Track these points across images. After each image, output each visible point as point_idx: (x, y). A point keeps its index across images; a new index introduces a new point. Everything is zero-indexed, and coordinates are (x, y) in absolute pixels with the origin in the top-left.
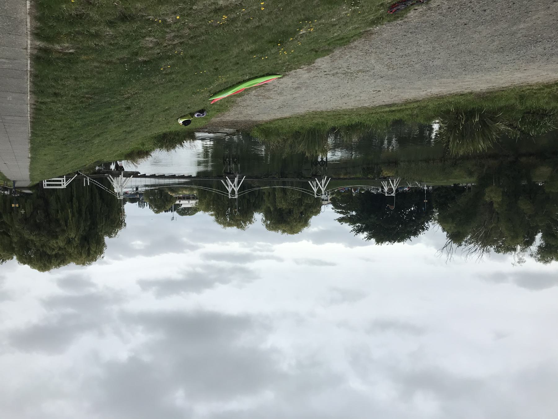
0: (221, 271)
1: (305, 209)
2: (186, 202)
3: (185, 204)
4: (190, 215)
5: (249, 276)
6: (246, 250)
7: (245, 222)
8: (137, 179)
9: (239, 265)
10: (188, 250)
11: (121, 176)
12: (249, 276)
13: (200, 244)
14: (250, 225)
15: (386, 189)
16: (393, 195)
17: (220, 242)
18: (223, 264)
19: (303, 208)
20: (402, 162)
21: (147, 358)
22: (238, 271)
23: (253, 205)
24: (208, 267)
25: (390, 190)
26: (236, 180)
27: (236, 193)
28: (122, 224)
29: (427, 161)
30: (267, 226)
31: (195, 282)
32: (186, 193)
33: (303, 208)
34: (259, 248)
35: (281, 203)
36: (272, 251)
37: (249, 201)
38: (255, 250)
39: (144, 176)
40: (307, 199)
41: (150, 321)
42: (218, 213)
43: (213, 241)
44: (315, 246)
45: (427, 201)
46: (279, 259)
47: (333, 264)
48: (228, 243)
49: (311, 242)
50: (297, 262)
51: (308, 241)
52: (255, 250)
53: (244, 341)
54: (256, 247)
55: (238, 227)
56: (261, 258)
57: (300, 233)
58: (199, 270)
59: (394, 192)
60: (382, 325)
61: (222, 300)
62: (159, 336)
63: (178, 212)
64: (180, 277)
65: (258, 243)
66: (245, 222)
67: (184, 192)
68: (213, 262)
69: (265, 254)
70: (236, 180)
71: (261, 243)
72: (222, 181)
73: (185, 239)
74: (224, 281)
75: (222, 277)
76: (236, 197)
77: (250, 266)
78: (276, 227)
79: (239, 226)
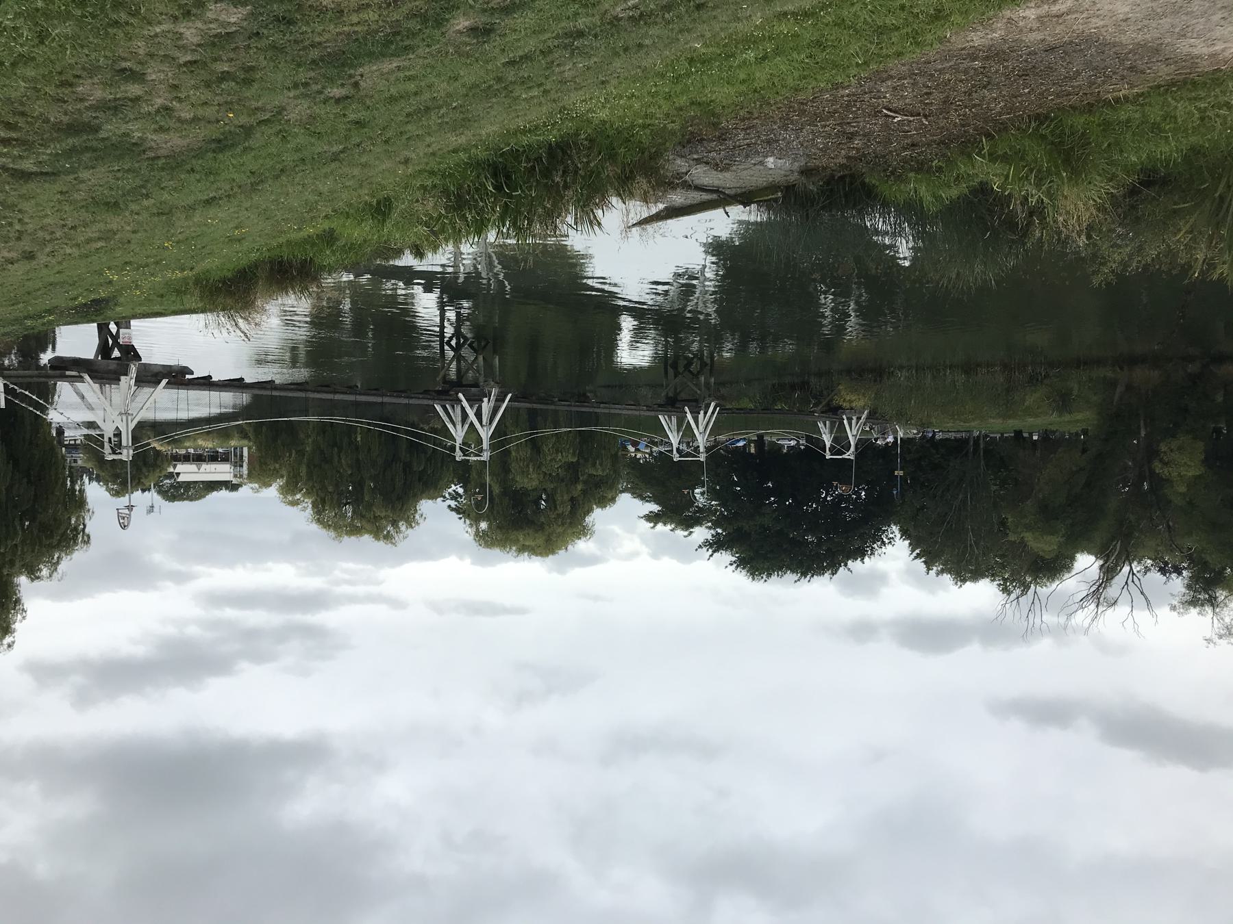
0: (251, 634)
1: (584, 492)
2: (191, 467)
3: (187, 472)
4: (191, 499)
5: (321, 643)
6: (314, 583)
7: (395, 524)
8: (183, 393)
9: (299, 618)
10: (169, 584)
11: (127, 381)
12: (321, 643)
13: (199, 568)
14: (410, 530)
15: (674, 439)
16: (850, 455)
17: (249, 565)
18: (256, 618)
19: (579, 487)
20: (901, 368)
21: (43, 869)
22: (294, 630)
23: (419, 480)
24: (215, 625)
25: (841, 443)
26: (486, 406)
27: (485, 445)
28: (75, 539)
29: (969, 368)
30: (477, 534)
31: (182, 661)
32: (207, 444)
33: (579, 487)
34: (347, 577)
35: (525, 473)
36: (379, 583)
37: (407, 467)
38: (338, 583)
39: (206, 383)
40: (594, 465)
41: (53, 766)
42: (323, 501)
43: (231, 564)
44: (478, 569)
45: (901, 473)
46: (396, 603)
47: (520, 611)
48: (270, 564)
49: (468, 561)
50: (437, 608)
51: (461, 558)
52: (338, 583)
53: (308, 805)
54: (338, 574)
55: (377, 537)
56: (353, 599)
57: (562, 552)
58: (193, 631)
59: (852, 449)
60: (628, 745)
61: (248, 705)
62: (77, 806)
63: (159, 492)
64: (140, 651)
65: (345, 565)
66: (395, 524)
67: (200, 442)
68: (230, 613)
69: (361, 590)
70: (486, 406)
71: (351, 565)
72: (438, 408)
73: (158, 557)
74: (259, 657)
75: (256, 646)
76: (485, 456)
77: (327, 618)
78: (507, 539)
79: (377, 533)
